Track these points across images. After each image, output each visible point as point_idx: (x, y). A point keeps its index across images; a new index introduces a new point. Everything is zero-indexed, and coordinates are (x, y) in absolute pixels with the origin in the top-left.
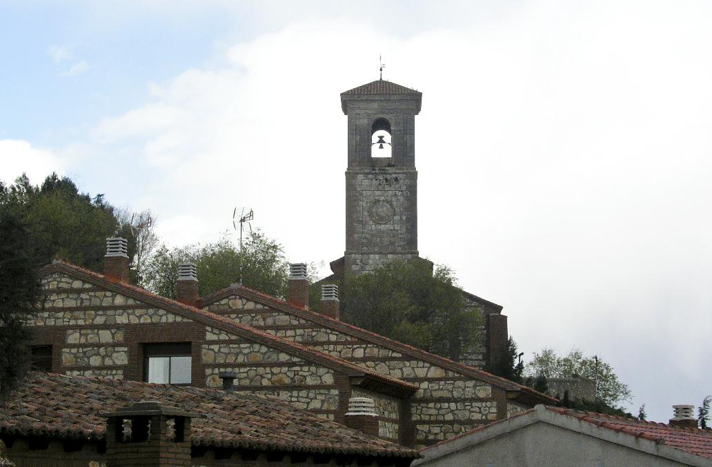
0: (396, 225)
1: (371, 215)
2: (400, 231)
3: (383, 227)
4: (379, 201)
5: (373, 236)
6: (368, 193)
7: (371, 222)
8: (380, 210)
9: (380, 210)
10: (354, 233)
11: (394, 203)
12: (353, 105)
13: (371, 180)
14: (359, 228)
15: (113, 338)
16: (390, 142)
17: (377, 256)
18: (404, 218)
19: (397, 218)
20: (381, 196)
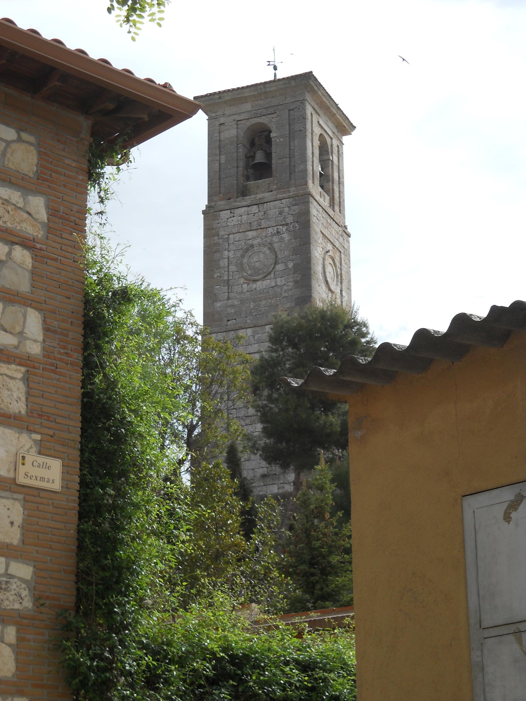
0: (278, 280)
1: (241, 268)
2: (285, 288)
3: (259, 285)
4: (252, 246)
5: (242, 301)
6: (238, 236)
7: (242, 281)
8: (255, 259)
9: (255, 259)
10: (216, 301)
11: (276, 246)
12: (216, 112)
13: (234, 400)
14: (221, 290)
15: (39, 493)
16: (278, 77)
17: (249, 331)
18: (291, 265)
19: (280, 267)
20: (254, 238)
